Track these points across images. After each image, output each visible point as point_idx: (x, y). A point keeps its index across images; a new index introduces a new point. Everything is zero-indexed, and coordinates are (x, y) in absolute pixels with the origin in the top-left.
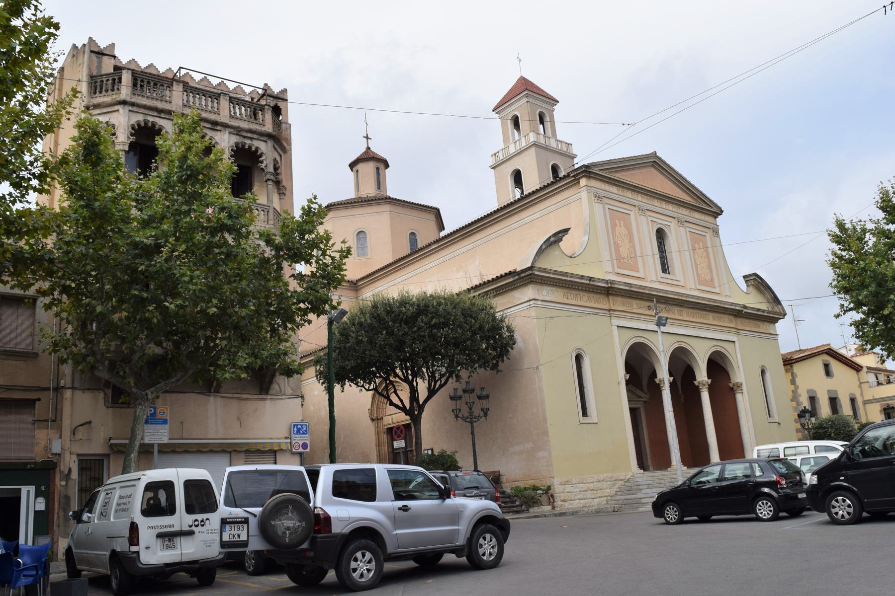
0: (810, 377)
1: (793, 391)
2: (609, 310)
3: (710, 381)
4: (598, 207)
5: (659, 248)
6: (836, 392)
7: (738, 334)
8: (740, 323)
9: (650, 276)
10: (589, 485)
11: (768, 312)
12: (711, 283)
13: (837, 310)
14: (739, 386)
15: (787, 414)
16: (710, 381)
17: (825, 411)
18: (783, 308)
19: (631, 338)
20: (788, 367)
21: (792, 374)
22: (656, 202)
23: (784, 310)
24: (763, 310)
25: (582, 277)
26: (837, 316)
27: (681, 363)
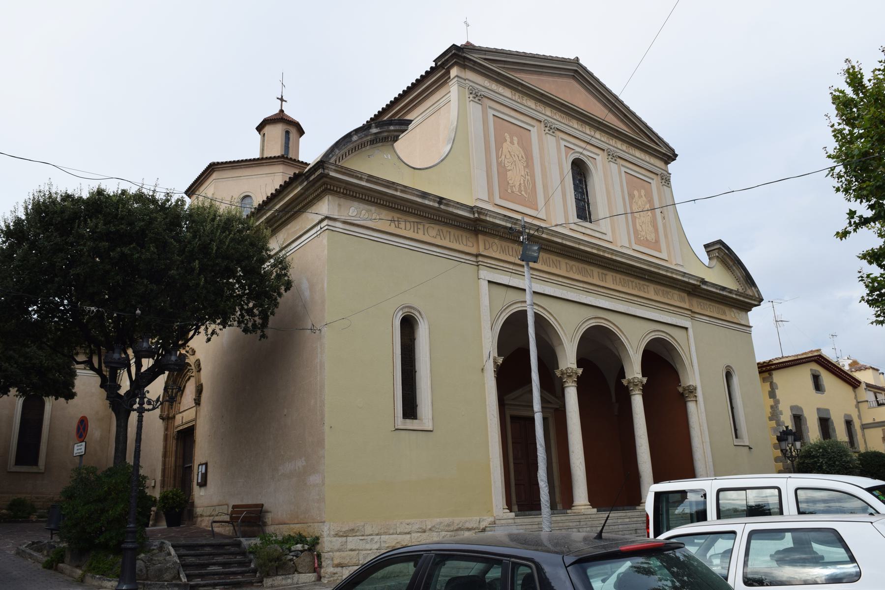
0: (795, 390)
1: (772, 407)
2: (477, 256)
3: (645, 380)
4: (474, 110)
5: (576, 187)
6: (827, 411)
7: (692, 318)
8: (696, 305)
9: (556, 213)
10: (400, 537)
11: (737, 293)
12: (656, 245)
13: (843, 223)
14: (692, 391)
15: (761, 434)
16: (645, 380)
17: (813, 434)
18: (758, 291)
19: (509, 304)
20: (766, 375)
21: (772, 384)
22: (575, 124)
23: (759, 294)
24: (732, 293)
25: (424, 195)
26: (844, 234)
27: (599, 347)
